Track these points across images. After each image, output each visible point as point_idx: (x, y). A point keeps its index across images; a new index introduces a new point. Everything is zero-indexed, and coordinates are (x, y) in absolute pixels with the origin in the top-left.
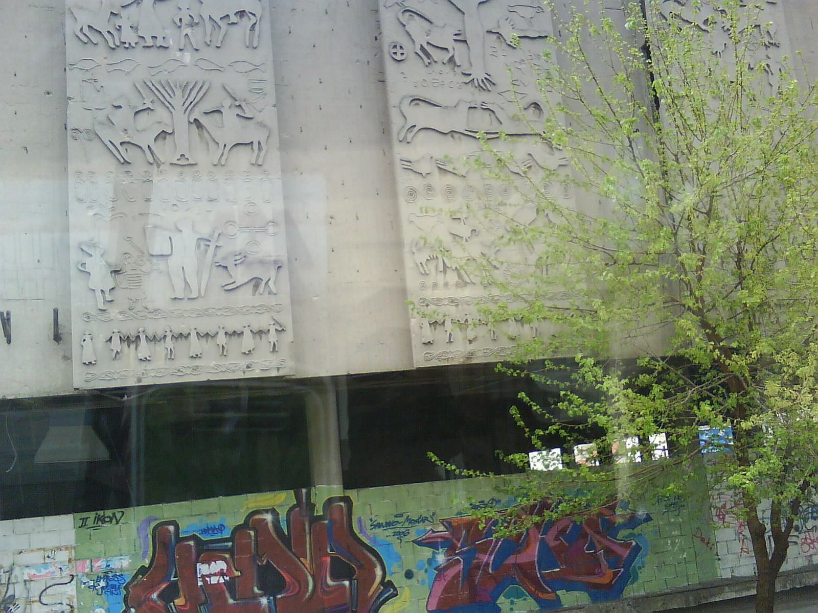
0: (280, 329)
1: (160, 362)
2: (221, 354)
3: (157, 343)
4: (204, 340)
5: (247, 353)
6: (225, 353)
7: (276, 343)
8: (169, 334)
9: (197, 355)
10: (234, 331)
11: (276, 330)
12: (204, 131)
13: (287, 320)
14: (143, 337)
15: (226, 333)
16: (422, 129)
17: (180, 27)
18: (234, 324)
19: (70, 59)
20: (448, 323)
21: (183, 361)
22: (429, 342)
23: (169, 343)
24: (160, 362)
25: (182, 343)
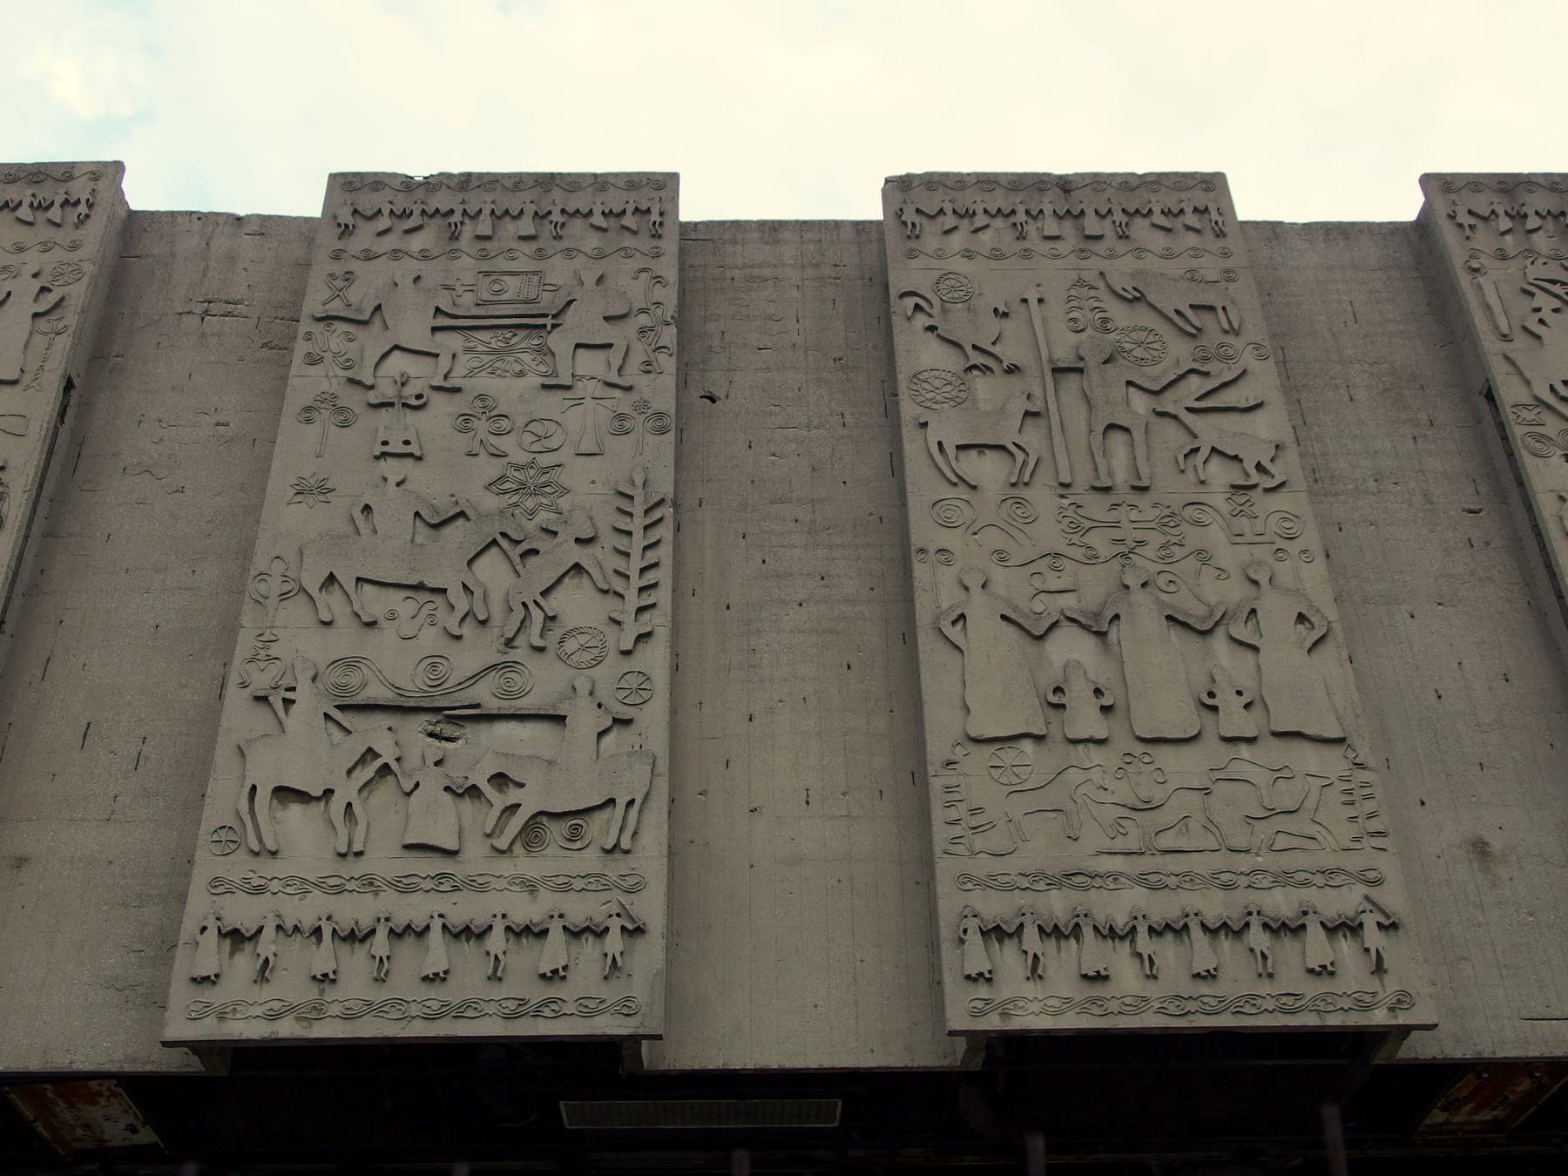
0: (1386, 923)
1: (404, 982)
2: (490, 971)
3: (357, 944)
4: (1053, 941)
5: (1318, 969)
6: (499, 974)
7: (501, 957)
8: (615, 924)
9: (1324, 967)
10: (409, 926)
11: (1378, 923)
12: (336, 583)
13: (651, 907)
14: (327, 933)
15: (508, 929)
16: (1188, 504)
17: (1183, 471)
18: (525, 911)
19: (917, 539)
20: (1031, 933)
21: (1291, 978)
23: (1258, 938)
25: (1288, 944)
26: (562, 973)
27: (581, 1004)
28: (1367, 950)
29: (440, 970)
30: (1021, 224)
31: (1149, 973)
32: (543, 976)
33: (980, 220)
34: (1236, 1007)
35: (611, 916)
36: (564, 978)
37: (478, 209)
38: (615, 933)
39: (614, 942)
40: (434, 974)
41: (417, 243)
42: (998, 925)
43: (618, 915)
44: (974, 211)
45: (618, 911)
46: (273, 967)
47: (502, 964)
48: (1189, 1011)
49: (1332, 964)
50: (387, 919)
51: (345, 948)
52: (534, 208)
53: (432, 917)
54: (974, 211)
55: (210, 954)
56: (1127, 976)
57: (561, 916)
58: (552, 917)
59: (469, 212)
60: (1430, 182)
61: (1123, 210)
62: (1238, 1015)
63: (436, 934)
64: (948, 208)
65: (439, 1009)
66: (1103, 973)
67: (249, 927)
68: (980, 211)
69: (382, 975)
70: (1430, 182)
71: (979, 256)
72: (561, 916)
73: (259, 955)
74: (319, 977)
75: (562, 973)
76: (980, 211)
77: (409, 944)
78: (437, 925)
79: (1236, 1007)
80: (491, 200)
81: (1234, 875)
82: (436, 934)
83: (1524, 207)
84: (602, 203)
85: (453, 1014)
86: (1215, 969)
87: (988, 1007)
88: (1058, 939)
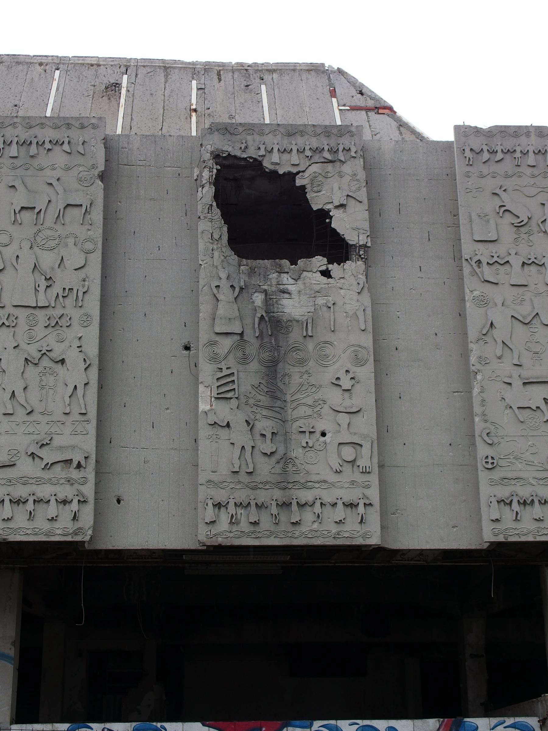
7: (32, 511)
22: (53, 518)
24: (266, 523)
26: (343, 521)
27: (293, 533)
28: (315, 513)
29: (54, 516)
30: (518, 158)
31: (275, 522)
32: (336, 522)
33: (500, 156)
34: (248, 535)
35: (74, 495)
36: (56, 520)
37: (271, 148)
38: (361, 506)
39: (75, 506)
40: (339, 521)
41: (500, 169)
42: (220, 502)
43: (77, 495)
44: (497, 151)
45: (77, 494)
46: (78, 517)
47: (33, 514)
48: (259, 537)
49: (258, 520)
50: (341, 498)
51: (61, 506)
52: (277, 147)
53: (52, 495)
54: (497, 151)
55: (210, 513)
56: (266, 523)
57: (55, 495)
58: (317, 499)
59: (346, 148)
60: (457, 128)
61: (471, 150)
62: (276, 538)
63: (53, 502)
64: (485, 148)
65: (39, 531)
66: (257, 522)
67: (224, 501)
68: (499, 151)
69: (277, 522)
70: (457, 128)
71: (346, 175)
72: (55, 495)
73: (229, 513)
74: (208, 523)
75: (343, 521)
76: (499, 151)
77: (42, 506)
78: (53, 499)
79: (248, 535)
80: (486, 143)
81: (313, 483)
82: (53, 502)
83: (546, 147)
84: (327, 145)
85: (44, 534)
86: (299, 521)
87: (41, 531)
88: (352, 508)
